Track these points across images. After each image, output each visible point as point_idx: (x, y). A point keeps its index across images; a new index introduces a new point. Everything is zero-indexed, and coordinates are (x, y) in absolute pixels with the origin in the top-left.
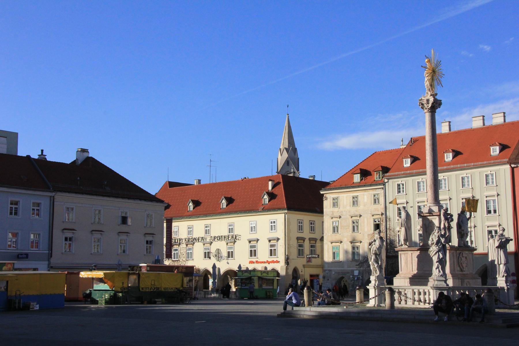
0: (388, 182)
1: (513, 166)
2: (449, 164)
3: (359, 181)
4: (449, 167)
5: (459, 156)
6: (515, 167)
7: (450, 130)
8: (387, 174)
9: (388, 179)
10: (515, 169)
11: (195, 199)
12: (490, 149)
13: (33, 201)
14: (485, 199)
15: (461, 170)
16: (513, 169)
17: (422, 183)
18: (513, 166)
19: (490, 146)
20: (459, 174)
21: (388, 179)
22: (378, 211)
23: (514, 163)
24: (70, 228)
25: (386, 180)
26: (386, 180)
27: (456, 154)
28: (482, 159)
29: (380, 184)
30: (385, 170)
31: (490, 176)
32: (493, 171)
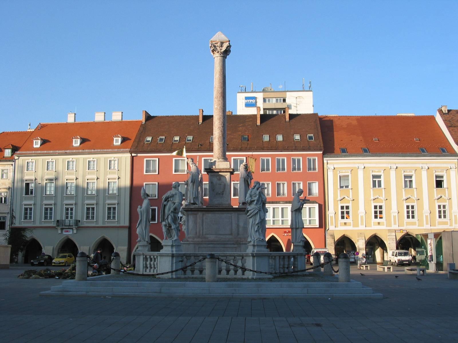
0: (18, 159)
1: (133, 155)
2: (77, 148)
3: (10, 155)
4: (119, 150)
5: (86, 143)
6: (134, 156)
7: (75, 121)
8: (18, 152)
9: (19, 157)
10: (134, 157)
11: (320, 203)
12: (73, 140)
13: (26, 171)
14: (108, 181)
15: (89, 154)
16: (132, 158)
17: (31, 163)
18: (133, 155)
19: (114, 137)
20: (86, 158)
21: (19, 157)
22: (6, 185)
23: (135, 153)
24: (292, 90)
25: (16, 158)
26: (16, 158)
27: (84, 141)
28: (105, 146)
29: (10, 161)
30: (15, 149)
31: (71, 162)
32: (117, 158)
